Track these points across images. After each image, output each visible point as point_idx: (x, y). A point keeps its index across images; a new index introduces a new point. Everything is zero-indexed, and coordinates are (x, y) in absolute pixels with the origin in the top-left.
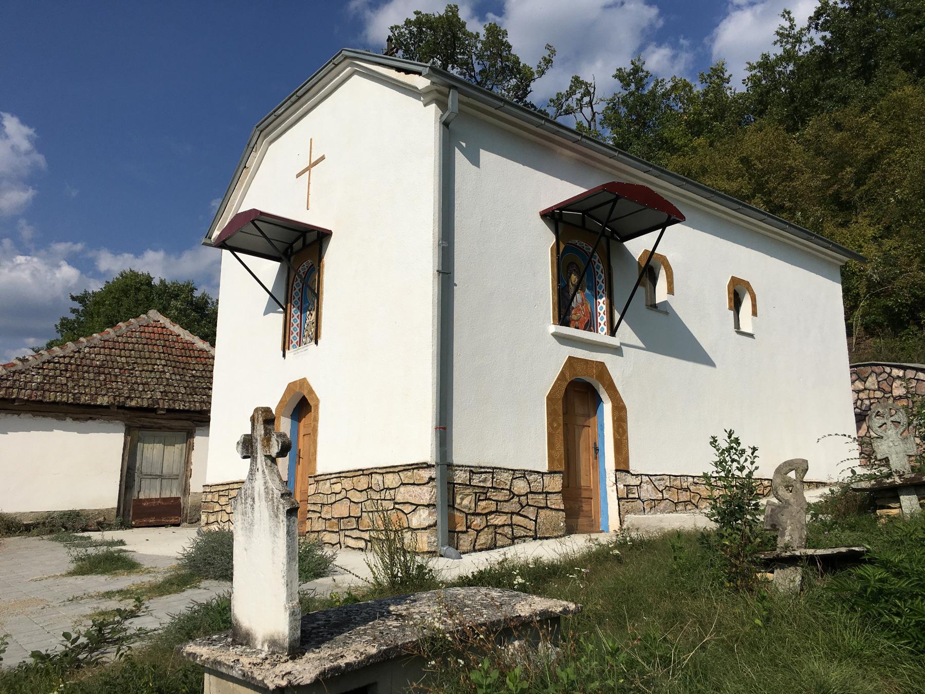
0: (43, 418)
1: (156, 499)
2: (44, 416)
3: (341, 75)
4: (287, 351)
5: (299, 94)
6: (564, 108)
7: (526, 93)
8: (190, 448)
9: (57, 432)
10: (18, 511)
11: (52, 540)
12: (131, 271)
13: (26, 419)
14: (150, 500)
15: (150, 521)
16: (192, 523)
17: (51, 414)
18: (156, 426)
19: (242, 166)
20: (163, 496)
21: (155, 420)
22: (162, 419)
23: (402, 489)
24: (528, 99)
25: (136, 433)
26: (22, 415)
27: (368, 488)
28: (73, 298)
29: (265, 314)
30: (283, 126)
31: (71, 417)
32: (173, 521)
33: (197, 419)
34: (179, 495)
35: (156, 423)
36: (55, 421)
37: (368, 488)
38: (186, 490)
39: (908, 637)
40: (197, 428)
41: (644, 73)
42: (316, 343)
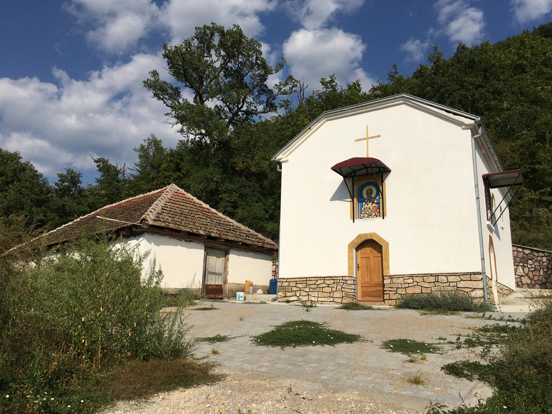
2: (174, 238)
3: (395, 103)
4: (355, 220)
5: (363, 105)
6: (282, 90)
7: (265, 80)
8: (227, 260)
13: (166, 239)
14: (211, 285)
15: (212, 296)
16: (229, 298)
17: (176, 237)
18: (215, 247)
19: (309, 127)
20: (216, 284)
21: (215, 244)
22: (217, 244)
23: (462, 282)
24: (265, 83)
26: (165, 237)
27: (435, 281)
29: (332, 199)
30: (342, 115)
32: (220, 297)
33: (230, 245)
34: (222, 284)
36: (178, 241)
37: (435, 281)
38: (225, 282)
41: (335, 84)
42: (383, 218)
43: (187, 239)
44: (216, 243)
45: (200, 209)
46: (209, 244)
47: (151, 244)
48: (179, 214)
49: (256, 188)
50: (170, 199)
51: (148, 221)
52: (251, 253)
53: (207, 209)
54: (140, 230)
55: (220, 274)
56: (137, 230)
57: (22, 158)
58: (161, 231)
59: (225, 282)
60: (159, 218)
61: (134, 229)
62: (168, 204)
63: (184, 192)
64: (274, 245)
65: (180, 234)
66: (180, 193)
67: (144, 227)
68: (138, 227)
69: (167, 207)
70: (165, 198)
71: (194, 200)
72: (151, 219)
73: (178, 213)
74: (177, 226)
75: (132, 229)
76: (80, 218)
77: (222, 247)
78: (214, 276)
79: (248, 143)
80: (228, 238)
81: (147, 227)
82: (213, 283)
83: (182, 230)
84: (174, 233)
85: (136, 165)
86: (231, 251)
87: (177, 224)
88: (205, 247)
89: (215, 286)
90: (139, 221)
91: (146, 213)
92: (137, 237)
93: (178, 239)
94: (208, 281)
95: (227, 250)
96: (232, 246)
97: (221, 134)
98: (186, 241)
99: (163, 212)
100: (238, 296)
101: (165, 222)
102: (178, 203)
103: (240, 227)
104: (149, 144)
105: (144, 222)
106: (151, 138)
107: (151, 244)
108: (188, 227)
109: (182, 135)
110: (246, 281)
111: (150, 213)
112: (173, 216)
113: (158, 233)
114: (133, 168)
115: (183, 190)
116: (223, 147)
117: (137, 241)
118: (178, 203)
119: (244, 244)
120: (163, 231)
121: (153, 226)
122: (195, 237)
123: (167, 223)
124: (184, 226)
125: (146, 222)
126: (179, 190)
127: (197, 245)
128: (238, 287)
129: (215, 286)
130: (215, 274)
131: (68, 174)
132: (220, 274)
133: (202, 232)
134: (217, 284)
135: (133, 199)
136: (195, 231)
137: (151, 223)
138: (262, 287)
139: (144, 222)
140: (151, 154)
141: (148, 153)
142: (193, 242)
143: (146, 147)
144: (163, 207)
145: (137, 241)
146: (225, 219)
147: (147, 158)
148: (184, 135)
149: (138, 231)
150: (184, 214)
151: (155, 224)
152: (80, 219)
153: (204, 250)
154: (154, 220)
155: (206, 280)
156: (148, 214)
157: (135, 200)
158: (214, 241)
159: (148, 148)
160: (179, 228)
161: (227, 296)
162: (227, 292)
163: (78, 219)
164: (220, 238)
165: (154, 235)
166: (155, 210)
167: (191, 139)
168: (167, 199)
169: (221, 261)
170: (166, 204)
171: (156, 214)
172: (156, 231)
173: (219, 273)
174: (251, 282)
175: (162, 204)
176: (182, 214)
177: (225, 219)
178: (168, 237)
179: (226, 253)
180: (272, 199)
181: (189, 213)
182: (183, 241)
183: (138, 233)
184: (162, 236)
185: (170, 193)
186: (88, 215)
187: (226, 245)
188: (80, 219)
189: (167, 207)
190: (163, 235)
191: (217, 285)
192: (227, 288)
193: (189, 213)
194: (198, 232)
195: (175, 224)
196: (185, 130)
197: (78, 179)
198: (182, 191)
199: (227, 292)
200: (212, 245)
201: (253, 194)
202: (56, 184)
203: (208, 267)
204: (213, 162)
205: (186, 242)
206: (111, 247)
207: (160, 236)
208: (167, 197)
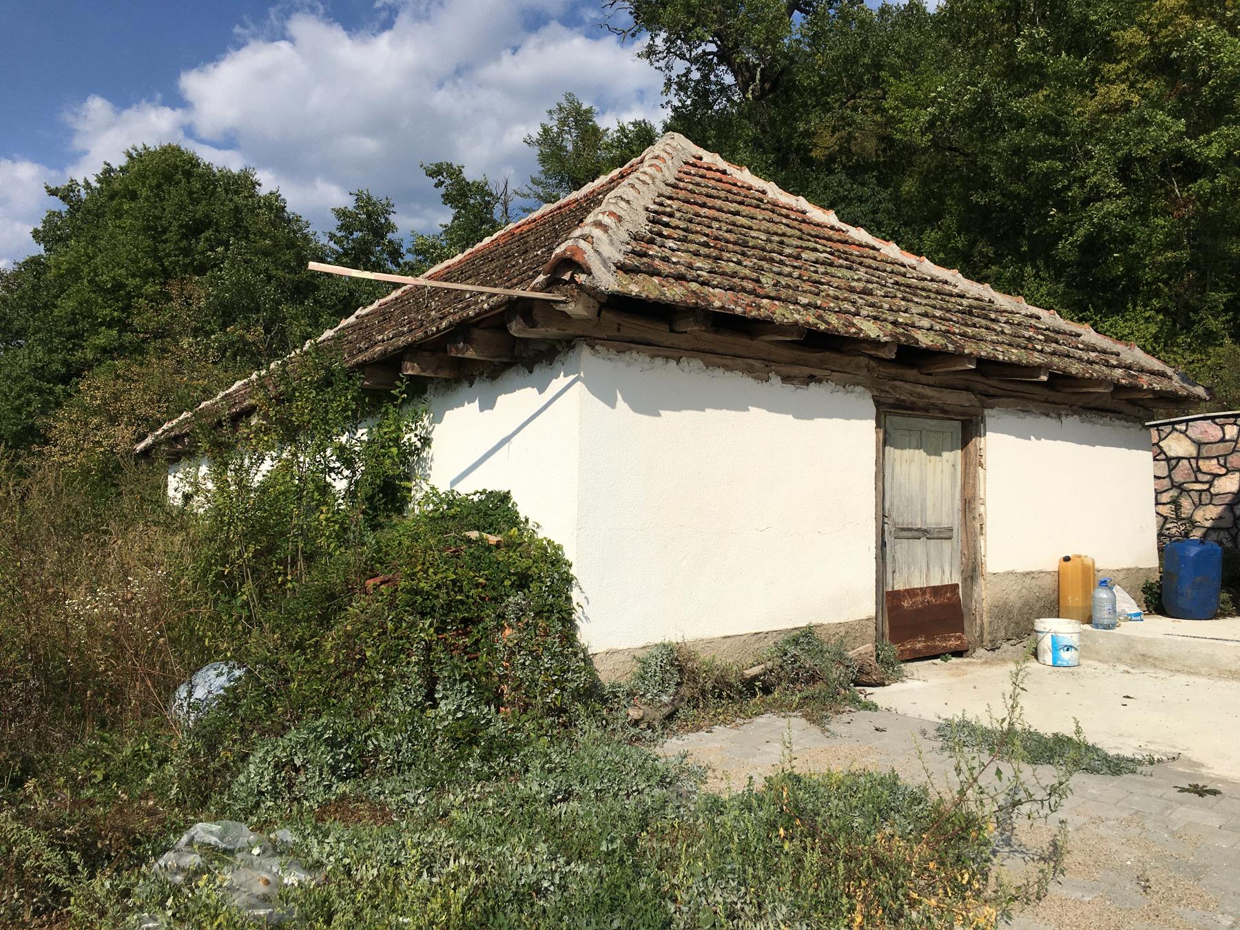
0: (728, 374)
1: (921, 589)
2: (728, 368)
9: (756, 414)
10: (699, 637)
11: (1201, 765)
12: (145, 148)
14: (911, 593)
15: (919, 646)
16: (993, 650)
17: (739, 361)
18: (921, 403)
20: (932, 585)
21: (919, 389)
25: (895, 421)
28: (53, 192)
31: (777, 373)
32: (953, 643)
33: (980, 387)
34: (956, 579)
35: (920, 396)
38: (972, 571)
39: (396, 630)
40: (986, 412)
43: (795, 370)
44: (924, 379)
45: (803, 226)
46: (894, 388)
47: (613, 405)
48: (730, 246)
49: (880, 202)
50: (675, 186)
51: (589, 273)
52: (1072, 422)
53: (832, 228)
54: (549, 331)
55: (944, 534)
56: (532, 334)
57: (260, 185)
58: (657, 332)
59: (974, 570)
60: (645, 260)
61: (516, 328)
62: (669, 202)
63: (722, 164)
64: (1163, 374)
65: (755, 343)
66: (709, 169)
67: (571, 308)
68: (537, 313)
69: (671, 215)
70: (653, 178)
71: (770, 195)
72: (604, 262)
73: (727, 241)
74: (747, 299)
75: (506, 330)
76: (358, 312)
77: (953, 399)
78: (919, 546)
79: (851, 60)
80: (985, 351)
81: (587, 307)
82: (918, 582)
83: (778, 318)
84: (728, 340)
85: (534, 181)
86: (992, 417)
87: (744, 290)
88: (878, 404)
89: (928, 596)
90: (541, 278)
91: (577, 232)
92: (537, 370)
93: (750, 371)
94: (897, 575)
95: (972, 410)
96: (992, 391)
97: (773, 39)
98: (786, 379)
99: (660, 235)
100: (1046, 643)
101: (680, 278)
102: (710, 202)
103: (990, 301)
104: (563, 122)
105: (566, 277)
106: (565, 104)
107: (613, 405)
108: (796, 303)
109: (652, 65)
110: (1067, 559)
111: (597, 232)
112: (715, 253)
113: (648, 344)
114: (526, 191)
115: (717, 156)
116: (772, 89)
117: (541, 391)
118: (710, 202)
119: (1060, 380)
120: (672, 331)
121: (618, 303)
122: (828, 354)
123: (694, 286)
124: (779, 299)
125: (581, 278)
126: (701, 159)
127: (841, 398)
128: (1030, 590)
129: (928, 596)
130: (924, 533)
131: (357, 207)
132: (944, 534)
133: (871, 329)
134: (935, 582)
135: (519, 227)
136: (833, 319)
137: (608, 281)
138: (1122, 575)
139: (566, 277)
140: (570, 147)
141: (562, 148)
142: (819, 381)
143: (555, 130)
144: (655, 212)
145: (541, 391)
146: (914, 268)
147: (561, 160)
148: (657, 64)
149: (543, 340)
150: (753, 248)
151: (634, 289)
152: (357, 317)
153: (873, 423)
154: (622, 268)
155: (889, 570)
156: (585, 238)
157: (526, 228)
158: (915, 372)
159: (560, 134)
160: (759, 307)
161: (987, 637)
162: (986, 619)
163: (352, 319)
164: (959, 356)
165: (626, 357)
166: (619, 219)
167: (678, 76)
168: (662, 186)
169: (947, 468)
170: (661, 204)
171: (626, 238)
172: (634, 334)
173: (940, 530)
174: (1088, 562)
175: (647, 198)
176: (745, 244)
177: (914, 268)
178: (697, 363)
179: (969, 430)
180: (940, 229)
181: (771, 241)
182: (776, 380)
183: (543, 347)
184: (667, 358)
185: (670, 163)
186: (382, 301)
187: (967, 389)
188: (357, 317)
189: (671, 215)
190: (674, 353)
191: (936, 591)
192: (985, 596)
193: (771, 241)
194: (854, 325)
195: (731, 289)
196: (660, 49)
197: (386, 219)
198: (709, 158)
199: (986, 619)
200: (904, 391)
201: (872, 220)
202: (331, 236)
203: (892, 504)
204: (748, 135)
205: (789, 388)
206: (426, 422)
207: (659, 362)
208: (659, 175)
